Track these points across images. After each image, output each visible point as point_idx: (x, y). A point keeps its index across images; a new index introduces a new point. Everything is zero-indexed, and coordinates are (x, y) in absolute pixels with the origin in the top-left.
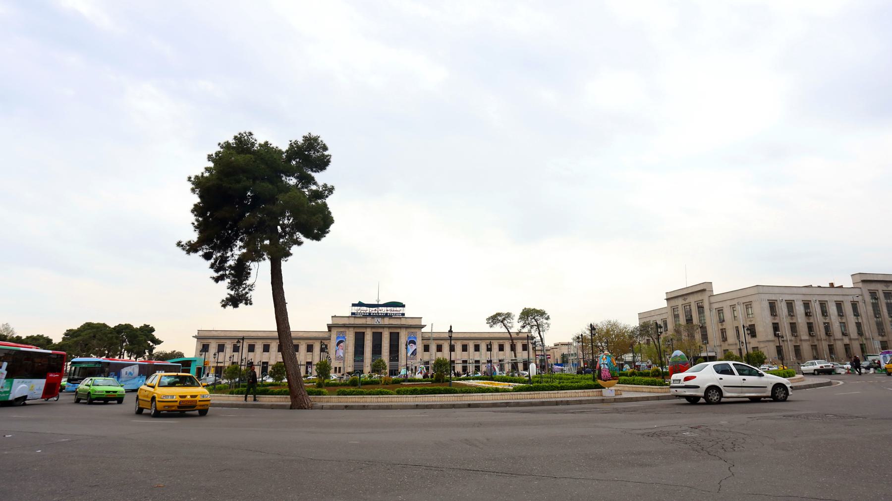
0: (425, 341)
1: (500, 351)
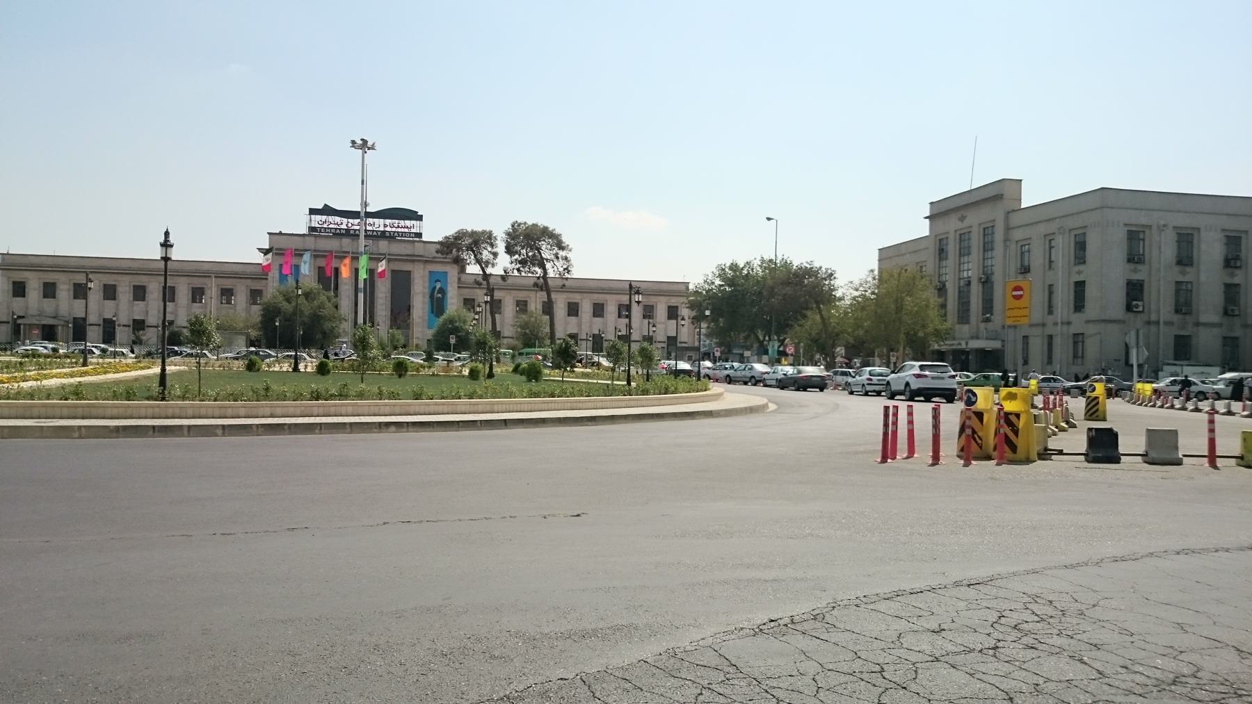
1: (15, 295)
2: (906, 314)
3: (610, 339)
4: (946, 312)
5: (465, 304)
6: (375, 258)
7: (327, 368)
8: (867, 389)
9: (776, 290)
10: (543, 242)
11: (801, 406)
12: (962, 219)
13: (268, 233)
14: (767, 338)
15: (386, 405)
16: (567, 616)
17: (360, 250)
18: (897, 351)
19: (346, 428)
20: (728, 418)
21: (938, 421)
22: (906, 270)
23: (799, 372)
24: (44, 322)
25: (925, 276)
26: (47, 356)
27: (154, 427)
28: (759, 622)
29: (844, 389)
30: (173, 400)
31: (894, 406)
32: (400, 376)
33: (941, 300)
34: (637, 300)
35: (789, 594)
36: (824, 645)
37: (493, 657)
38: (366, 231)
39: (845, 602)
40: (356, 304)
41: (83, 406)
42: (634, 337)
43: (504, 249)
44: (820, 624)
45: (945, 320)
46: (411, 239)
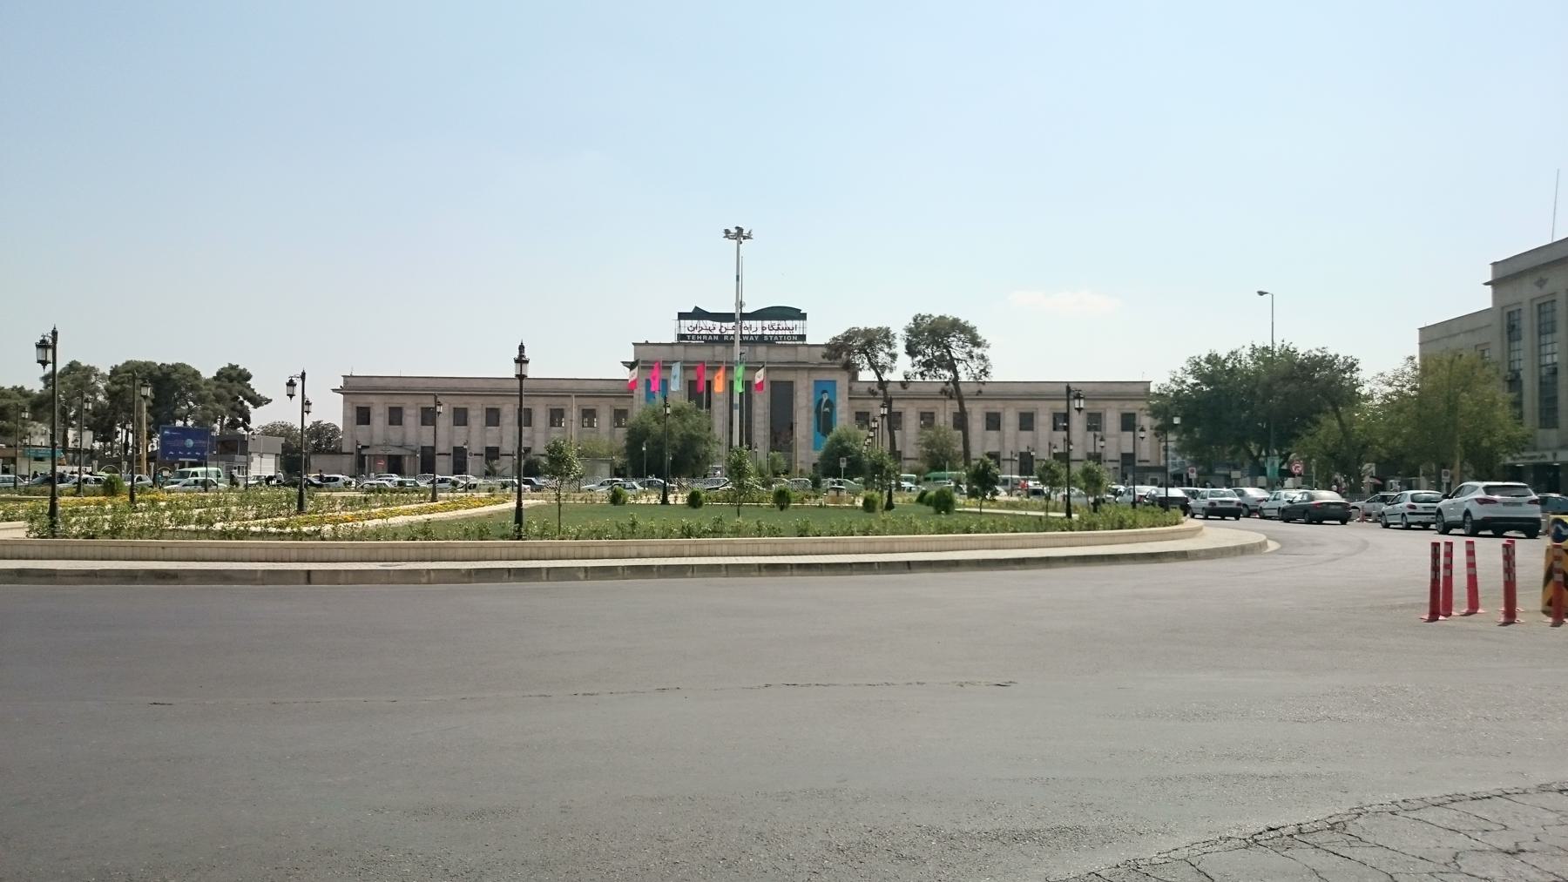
0: (858, 403)
2: (1462, 416)
3: (1042, 458)
4: (1522, 412)
5: (857, 419)
6: (752, 368)
7: (699, 500)
8: (1409, 520)
9: (1275, 387)
10: (952, 339)
11: (1314, 545)
12: (1541, 283)
13: (634, 344)
14: (1264, 453)
15: (766, 543)
16: (993, 812)
17: (735, 359)
18: (1451, 468)
19: (721, 571)
20: (1210, 561)
21: (1511, 562)
22: (1461, 356)
23: (1311, 498)
24: (389, 453)
25: (1488, 363)
26: (393, 491)
27: (509, 570)
28: (1253, 831)
29: (1376, 521)
30: (530, 539)
31: (1447, 543)
32: (782, 508)
33: (1512, 396)
34: (1077, 407)
35: (1295, 795)
36: (1344, 863)
37: (901, 857)
38: (741, 335)
39: (1375, 808)
40: (731, 424)
41: (431, 547)
42: (1074, 456)
43: (904, 350)
44: (1339, 835)
45: (1521, 424)
46: (794, 343)
